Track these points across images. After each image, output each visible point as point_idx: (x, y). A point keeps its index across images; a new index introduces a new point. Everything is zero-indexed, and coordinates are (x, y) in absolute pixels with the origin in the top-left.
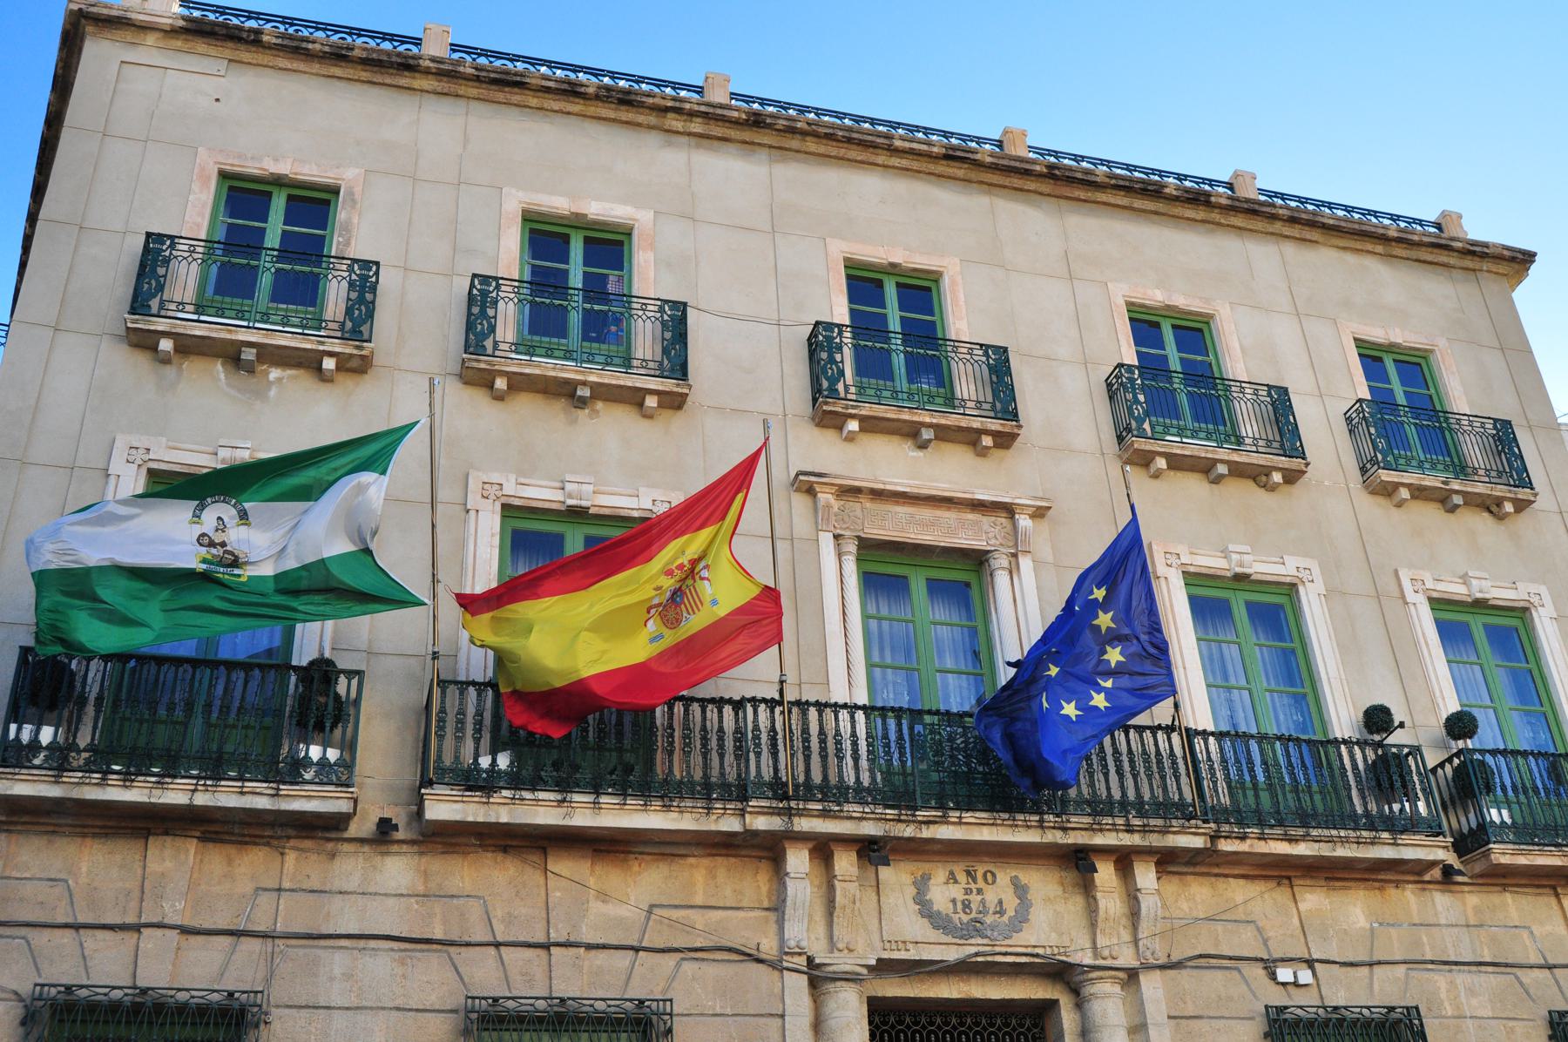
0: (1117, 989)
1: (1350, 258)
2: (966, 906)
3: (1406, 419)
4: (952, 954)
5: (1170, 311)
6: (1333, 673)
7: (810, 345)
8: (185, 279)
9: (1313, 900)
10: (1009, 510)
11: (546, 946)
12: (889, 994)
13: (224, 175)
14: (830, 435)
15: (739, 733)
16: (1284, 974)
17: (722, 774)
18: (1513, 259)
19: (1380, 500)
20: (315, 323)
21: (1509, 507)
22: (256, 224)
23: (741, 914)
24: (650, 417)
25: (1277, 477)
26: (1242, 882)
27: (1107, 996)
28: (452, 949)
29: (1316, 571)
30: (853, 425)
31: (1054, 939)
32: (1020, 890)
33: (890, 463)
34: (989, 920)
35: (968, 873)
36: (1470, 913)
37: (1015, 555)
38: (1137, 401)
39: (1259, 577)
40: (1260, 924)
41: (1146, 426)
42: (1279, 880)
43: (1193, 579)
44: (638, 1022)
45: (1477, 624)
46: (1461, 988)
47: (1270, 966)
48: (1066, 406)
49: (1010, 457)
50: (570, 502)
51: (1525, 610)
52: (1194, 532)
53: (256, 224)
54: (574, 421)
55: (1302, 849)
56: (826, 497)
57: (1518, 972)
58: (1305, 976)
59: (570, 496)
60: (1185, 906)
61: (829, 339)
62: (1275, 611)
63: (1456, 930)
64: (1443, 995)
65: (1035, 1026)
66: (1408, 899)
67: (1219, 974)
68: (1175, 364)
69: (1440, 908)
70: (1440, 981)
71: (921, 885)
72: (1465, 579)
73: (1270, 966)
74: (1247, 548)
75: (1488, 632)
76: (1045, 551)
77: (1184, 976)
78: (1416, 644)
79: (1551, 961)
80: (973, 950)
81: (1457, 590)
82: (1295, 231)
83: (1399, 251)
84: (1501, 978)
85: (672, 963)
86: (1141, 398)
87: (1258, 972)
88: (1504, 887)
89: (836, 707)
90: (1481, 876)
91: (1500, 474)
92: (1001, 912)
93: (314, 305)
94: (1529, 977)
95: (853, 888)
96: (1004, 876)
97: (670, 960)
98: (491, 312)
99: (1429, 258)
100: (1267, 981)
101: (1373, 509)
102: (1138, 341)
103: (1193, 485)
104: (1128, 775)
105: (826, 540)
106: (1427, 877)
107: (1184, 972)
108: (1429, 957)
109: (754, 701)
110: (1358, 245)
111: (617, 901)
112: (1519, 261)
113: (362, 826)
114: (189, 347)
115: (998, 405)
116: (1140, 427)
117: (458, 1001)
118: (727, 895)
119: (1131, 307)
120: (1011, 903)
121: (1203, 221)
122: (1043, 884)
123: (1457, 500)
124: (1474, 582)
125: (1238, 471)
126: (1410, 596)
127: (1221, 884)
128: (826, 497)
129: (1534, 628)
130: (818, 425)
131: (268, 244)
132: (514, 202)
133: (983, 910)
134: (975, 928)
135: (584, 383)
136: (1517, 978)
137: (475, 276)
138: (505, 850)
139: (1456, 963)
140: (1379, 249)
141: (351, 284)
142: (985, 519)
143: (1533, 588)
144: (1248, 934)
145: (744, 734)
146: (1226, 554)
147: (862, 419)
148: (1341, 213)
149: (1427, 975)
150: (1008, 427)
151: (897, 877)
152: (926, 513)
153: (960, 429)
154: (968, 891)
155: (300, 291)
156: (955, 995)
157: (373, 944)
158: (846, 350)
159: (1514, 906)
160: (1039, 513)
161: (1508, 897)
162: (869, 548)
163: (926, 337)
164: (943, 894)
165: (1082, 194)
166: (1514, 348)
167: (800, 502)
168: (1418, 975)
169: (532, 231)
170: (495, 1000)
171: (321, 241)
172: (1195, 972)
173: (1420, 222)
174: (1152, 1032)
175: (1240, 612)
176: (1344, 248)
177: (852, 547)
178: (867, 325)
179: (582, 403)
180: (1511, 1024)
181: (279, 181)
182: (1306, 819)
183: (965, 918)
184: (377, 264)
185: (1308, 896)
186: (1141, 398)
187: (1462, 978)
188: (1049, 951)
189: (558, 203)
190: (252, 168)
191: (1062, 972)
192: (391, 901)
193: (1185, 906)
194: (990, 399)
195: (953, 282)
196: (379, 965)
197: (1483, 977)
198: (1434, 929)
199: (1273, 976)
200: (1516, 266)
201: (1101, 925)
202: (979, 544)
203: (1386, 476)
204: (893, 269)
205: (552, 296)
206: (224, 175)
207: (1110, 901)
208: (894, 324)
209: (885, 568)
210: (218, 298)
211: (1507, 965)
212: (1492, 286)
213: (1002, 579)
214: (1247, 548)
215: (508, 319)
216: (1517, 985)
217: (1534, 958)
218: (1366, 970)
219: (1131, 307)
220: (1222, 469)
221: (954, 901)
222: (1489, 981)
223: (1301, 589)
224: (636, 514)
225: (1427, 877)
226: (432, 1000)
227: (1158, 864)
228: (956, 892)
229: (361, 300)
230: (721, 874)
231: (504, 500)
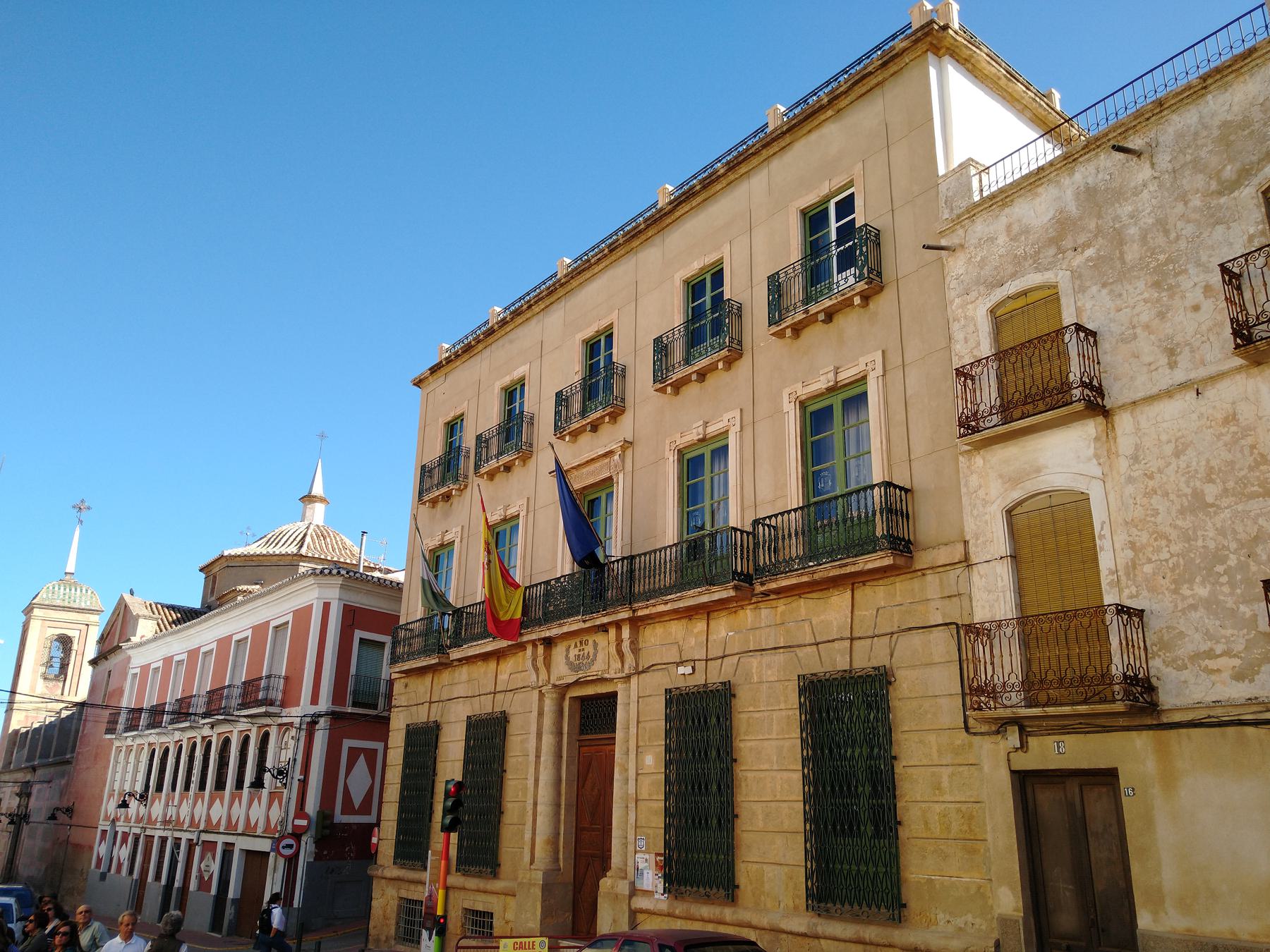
1: (814, 136)
57: (797, 650)
67: (660, 673)
88: (800, 596)
94: (801, 652)
99: (864, 89)
110: (816, 122)
140: (830, 113)
165: (669, 221)
176: (810, 131)
187: (767, 658)
218: (869, 641)
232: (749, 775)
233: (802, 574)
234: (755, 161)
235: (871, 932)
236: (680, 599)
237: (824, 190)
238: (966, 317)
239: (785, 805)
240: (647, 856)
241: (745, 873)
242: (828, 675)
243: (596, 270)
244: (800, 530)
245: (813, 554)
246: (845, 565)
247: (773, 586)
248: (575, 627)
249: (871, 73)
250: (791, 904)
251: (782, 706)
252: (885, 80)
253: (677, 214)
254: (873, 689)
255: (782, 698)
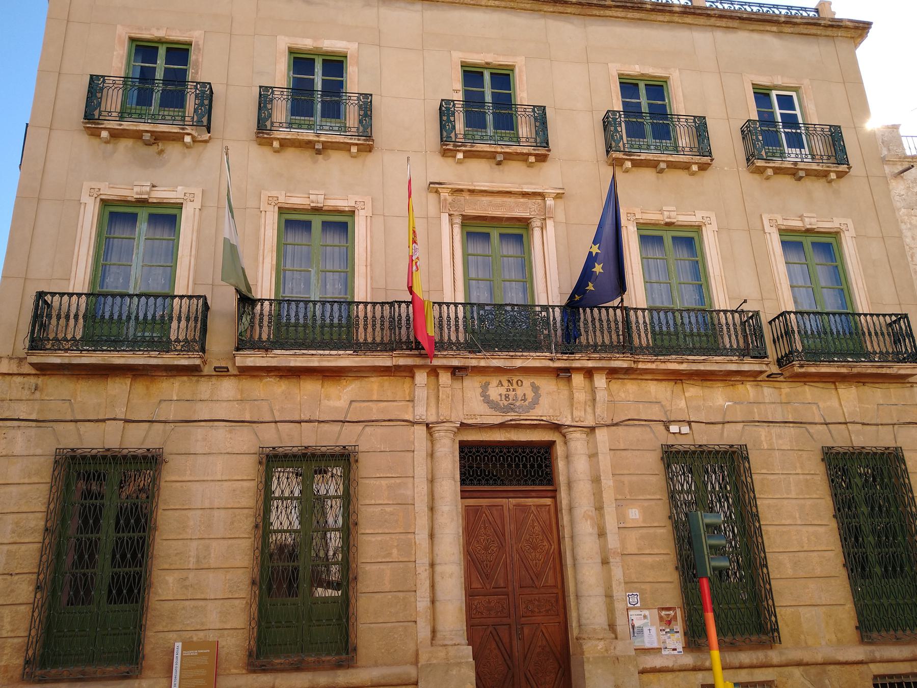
0: (584, 436)
1: (756, 36)
2: (507, 397)
3: (773, 130)
4: (499, 420)
5: (642, 77)
6: (717, 272)
7: (604, 122)
8: (113, 101)
9: (693, 391)
10: (542, 195)
11: (299, 422)
12: (470, 439)
13: (132, 40)
14: (450, 160)
15: (392, 318)
16: (674, 428)
17: (449, 338)
18: (856, 28)
19: (756, 176)
20: (515, 139)
21: (833, 176)
22: (147, 65)
23: (395, 404)
24: (355, 157)
25: (695, 168)
26: (655, 382)
27: (578, 439)
28: (254, 425)
29: (713, 219)
30: (460, 156)
31: (551, 412)
32: (535, 389)
33: (480, 175)
34: (518, 404)
35: (509, 381)
36: (783, 396)
37: (545, 219)
38: (758, 140)
39: (680, 223)
40: (663, 403)
41: (763, 153)
42: (676, 381)
43: (640, 226)
44: (342, 455)
45: (807, 241)
46: (774, 435)
47: (666, 424)
48: (577, 137)
49: (546, 167)
50: (312, 205)
51: (700, 227)
52: (648, 200)
53: (147, 65)
54: (315, 162)
55: (684, 367)
56: (445, 195)
57: (808, 426)
58: (685, 429)
59: (313, 202)
60: (623, 395)
61: (448, 109)
62: (688, 241)
63: (774, 405)
64: (763, 438)
65: (546, 452)
66: (748, 390)
67: (639, 429)
68: (645, 108)
69: (766, 394)
70: (762, 432)
71: (485, 387)
72: (801, 218)
73: (666, 424)
74: (674, 208)
75: (814, 248)
76: (560, 216)
77: (620, 430)
78: (768, 255)
79: (828, 421)
80: (510, 418)
81: (796, 224)
82: (723, 23)
83: (787, 29)
84: (798, 430)
85: (361, 428)
86: (760, 138)
87: (661, 427)
88: (805, 383)
89: (448, 304)
90: (789, 377)
91: (829, 157)
92: (525, 400)
93: (339, 117)
94: (813, 429)
95: (448, 390)
96: (527, 382)
97: (359, 427)
98: (452, 119)
99: (805, 31)
100: (665, 432)
101: (751, 181)
102: (758, 105)
103: (648, 174)
104: (606, 332)
105: (445, 218)
106: (759, 379)
107: (620, 428)
108: (757, 419)
109: (400, 303)
110: (761, 28)
111: (338, 398)
112: (861, 29)
113: (207, 370)
114: (115, 135)
115: (195, 119)
116: (617, 145)
117: (361, 449)
118: (389, 395)
119: (621, 76)
120: (530, 395)
121: (669, 22)
122: (547, 385)
123: (802, 173)
124: (806, 219)
125: (672, 165)
126: (767, 229)
127: (643, 383)
128: (445, 195)
129: (841, 243)
130: (443, 156)
131: (157, 77)
132: (284, 43)
133: (516, 399)
134: (510, 408)
135: (319, 142)
136: (807, 429)
137: (442, 100)
138: (281, 377)
139: (772, 422)
140: (774, 29)
141: (360, 107)
142: (530, 201)
143: (843, 221)
144: (656, 408)
145: (394, 319)
146: (661, 211)
147: (464, 152)
148: (755, 9)
149: (755, 428)
150: (542, 151)
151: (472, 385)
152: (498, 200)
153: (517, 154)
154: (508, 390)
155: (333, 110)
156: (503, 439)
157: (216, 424)
158: (623, 124)
159: (808, 392)
160: (558, 196)
161: (807, 388)
162: (467, 220)
163: (661, 113)
164: (495, 392)
165: (597, 13)
166: (852, 80)
167: (432, 197)
168: (751, 429)
169: (464, 71)
170: (274, 448)
171: (185, 72)
172: (625, 428)
173: (805, 9)
174: (601, 457)
175: (668, 241)
176: (753, 30)
177: (458, 220)
178: (472, 100)
179: (319, 152)
180: (800, 453)
181: (160, 41)
182: (843, 355)
183: (506, 403)
184: (371, 95)
185: (691, 389)
186: (760, 138)
187: (775, 430)
188: (548, 418)
189: (306, 43)
190: (146, 35)
191: (556, 427)
192: (225, 404)
193: (623, 395)
194: (697, 145)
195: (521, 71)
196: (220, 433)
197: (787, 430)
198: (762, 406)
199: (668, 429)
200: (860, 32)
201: (575, 406)
202: (526, 215)
203: (760, 163)
204: (487, 66)
205: (636, 117)
206: (132, 40)
207: (581, 396)
208: (488, 98)
209: (475, 230)
210: (139, 107)
211: (801, 423)
212: (843, 46)
213: (537, 233)
214: (674, 208)
215: (280, 111)
216: (807, 433)
217: (818, 419)
218: (720, 426)
219: (621, 76)
220: (663, 165)
221: (501, 395)
222: (791, 431)
223: (704, 228)
224: (347, 209)
225: (759, 379)
226: (245, 449)
227: (607, 374)
228: (502, 390)
229: (366, 115)
230: (386, 384)
231: (280, 205)
232: (770, 529)
233: (843, 366)
234: (702, 21)
235: (323, 678)
236: (704, 361)
237: (779, 81)
238: (911, 223)
239: (815, 554)
240: (647, 613)
241: (784, 616)
242: (94, 452)
243: (569, 10)
244: (192, 316)
245: (91, 341)
246: (882, 367)
247: (813, 370)
248: (537, 364)
249: (819, 25)
250: (834, 638)
251: (799, 471)
252: (820, 35)
253: (608, 13)
254: (732, 462)
255: (798, 465)
